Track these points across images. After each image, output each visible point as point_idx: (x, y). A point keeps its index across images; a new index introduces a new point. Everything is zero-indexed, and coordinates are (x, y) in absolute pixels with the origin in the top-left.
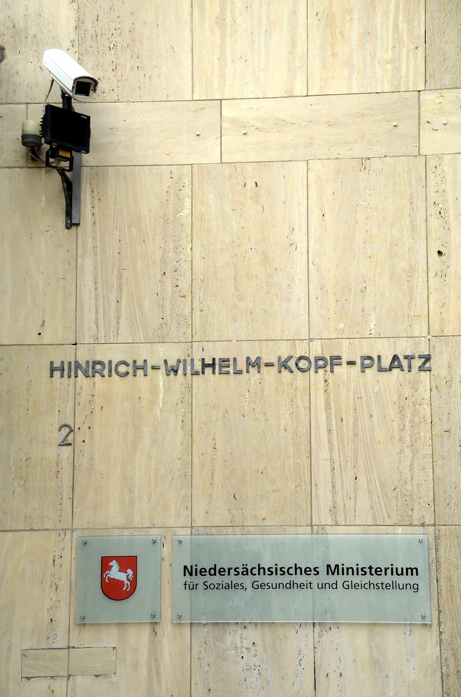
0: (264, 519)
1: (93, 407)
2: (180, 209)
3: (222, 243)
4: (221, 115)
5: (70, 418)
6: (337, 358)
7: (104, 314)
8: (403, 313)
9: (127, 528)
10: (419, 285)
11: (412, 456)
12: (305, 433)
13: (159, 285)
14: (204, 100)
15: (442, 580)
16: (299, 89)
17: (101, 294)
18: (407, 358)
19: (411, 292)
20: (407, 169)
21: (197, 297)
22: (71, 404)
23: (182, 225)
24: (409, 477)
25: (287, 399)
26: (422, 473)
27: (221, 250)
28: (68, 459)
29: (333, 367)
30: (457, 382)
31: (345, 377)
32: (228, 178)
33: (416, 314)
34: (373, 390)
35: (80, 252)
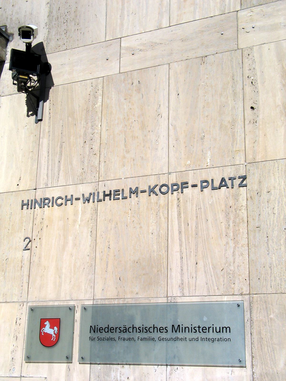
0: (137, 293)
1: (42, 226)
2: (96, 103)
3: (118, 119)
4: (120, 47)
5: (30, 233)
6: (185, 183)
7: (52, 170)
8: (228, 150)
9: (57, 301)
10: (239, 130)
11: (234, 246)
12: (164, 235)
13: (82, 149)
14: (112, 40)
15: (255, 334)
16: (165, 23)
17: (51, 158)
18: (231, 180)
19: (233, 135)
20: (230, 58)
21: (103, 154)
22: (31, 225)
23: (96, 112)
24: (232, 261)
25: (154, 212)
26: (241, 258)
27: (118, 124)
28: (27, 258)
29: (183, 189)
30: (265, 193)
31: (190, 196)
32: (123, 81)
33: (237, 150)
34: (208, 202)
35: (41, 135)
